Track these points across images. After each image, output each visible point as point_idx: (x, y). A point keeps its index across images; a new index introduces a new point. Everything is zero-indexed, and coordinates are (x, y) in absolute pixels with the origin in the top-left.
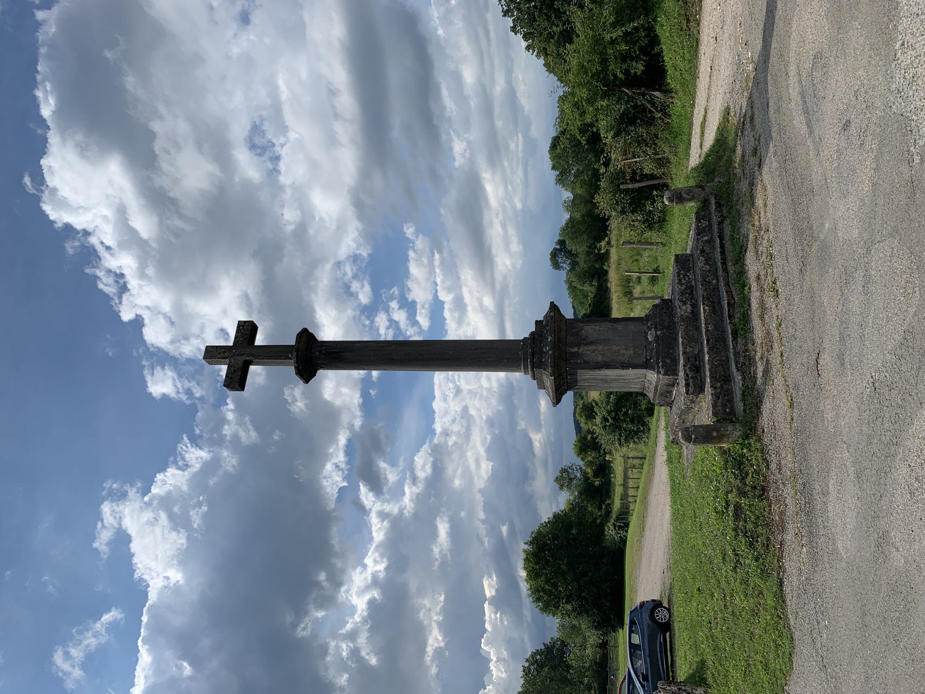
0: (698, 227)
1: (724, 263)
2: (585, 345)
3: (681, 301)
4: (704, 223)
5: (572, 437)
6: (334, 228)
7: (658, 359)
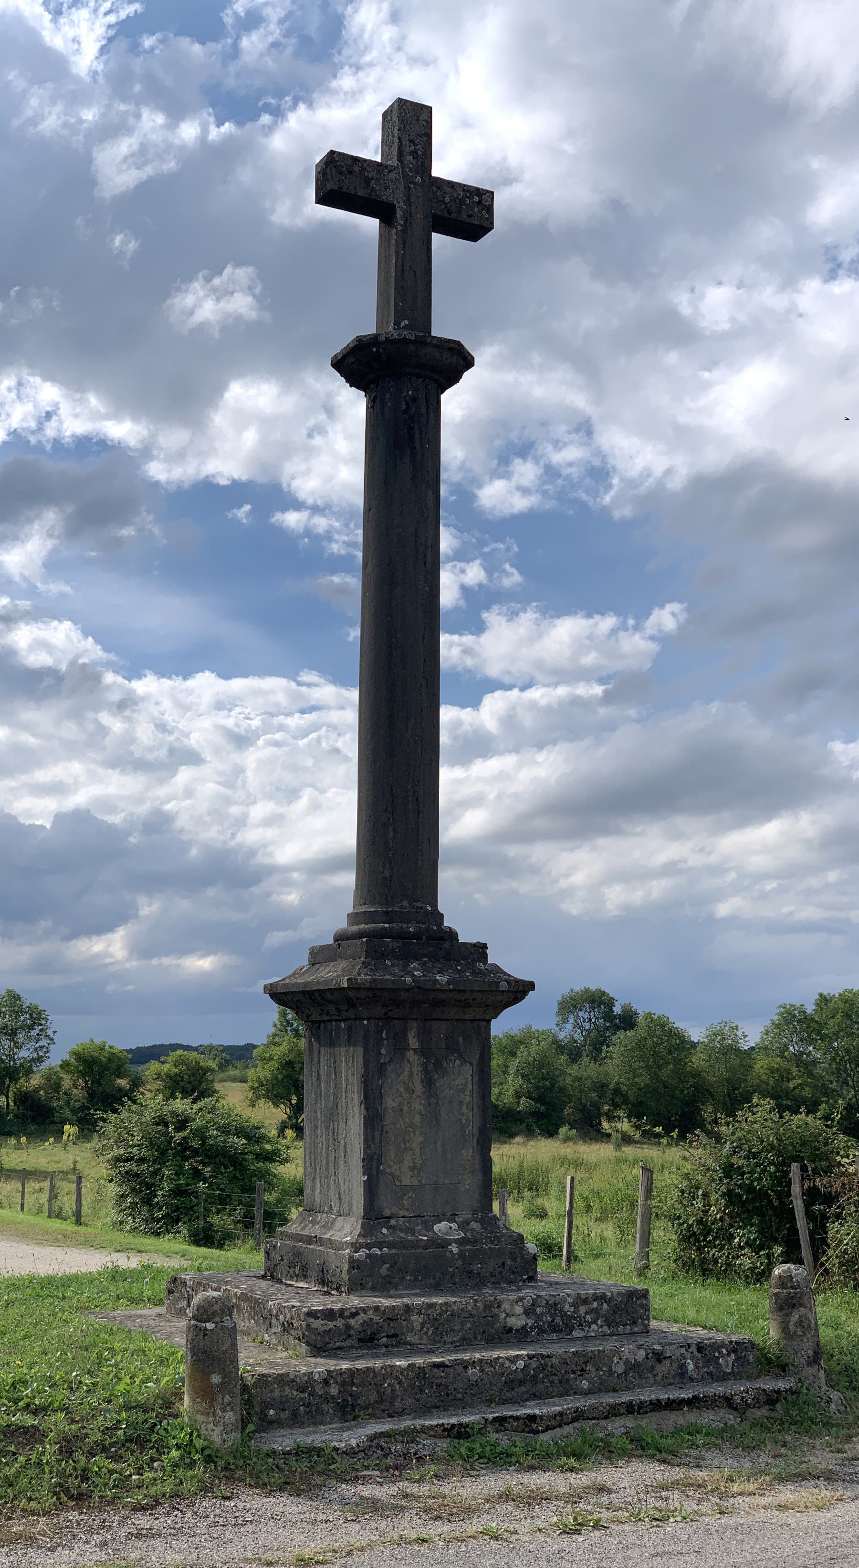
0: (717, 1346)
1: (631, 1409)
2: (425, 1067)
3: (534, 1304)
4: (727, 1362)
5: (122, 1038)
6: (682, 419)
7: (390, 1245)
